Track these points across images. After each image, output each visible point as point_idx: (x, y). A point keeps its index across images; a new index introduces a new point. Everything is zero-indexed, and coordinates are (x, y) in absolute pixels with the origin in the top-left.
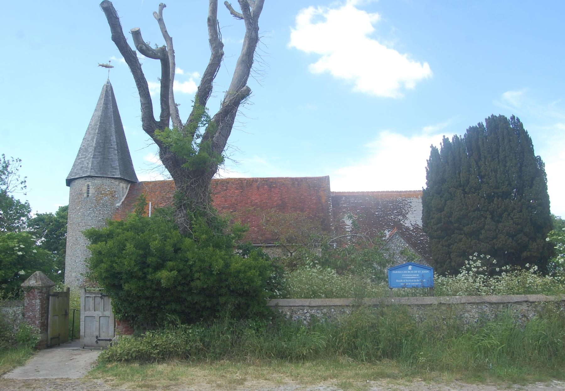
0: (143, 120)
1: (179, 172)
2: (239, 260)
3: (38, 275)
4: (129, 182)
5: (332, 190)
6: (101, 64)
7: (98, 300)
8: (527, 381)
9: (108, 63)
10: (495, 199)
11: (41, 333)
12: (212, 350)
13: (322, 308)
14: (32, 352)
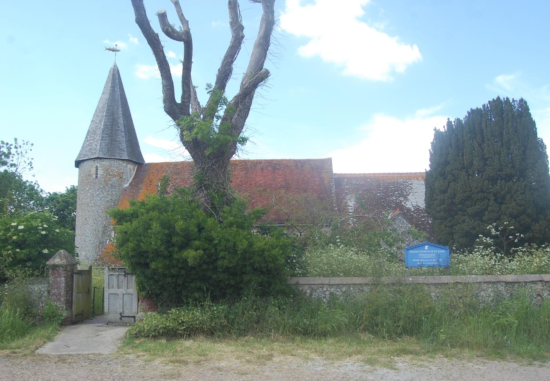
0: (165, 102)
1: (199, 153)
2: (262, 241)
3: (63, 253)
5: (334, 172)
6: (108, 48)
7: (122, 278)
8: (547, 358)
9: (115, 47)
10: (499, 181)
11: (66, 310)
12: (237, 327)
13: (341, 286)
14: (58, 327)
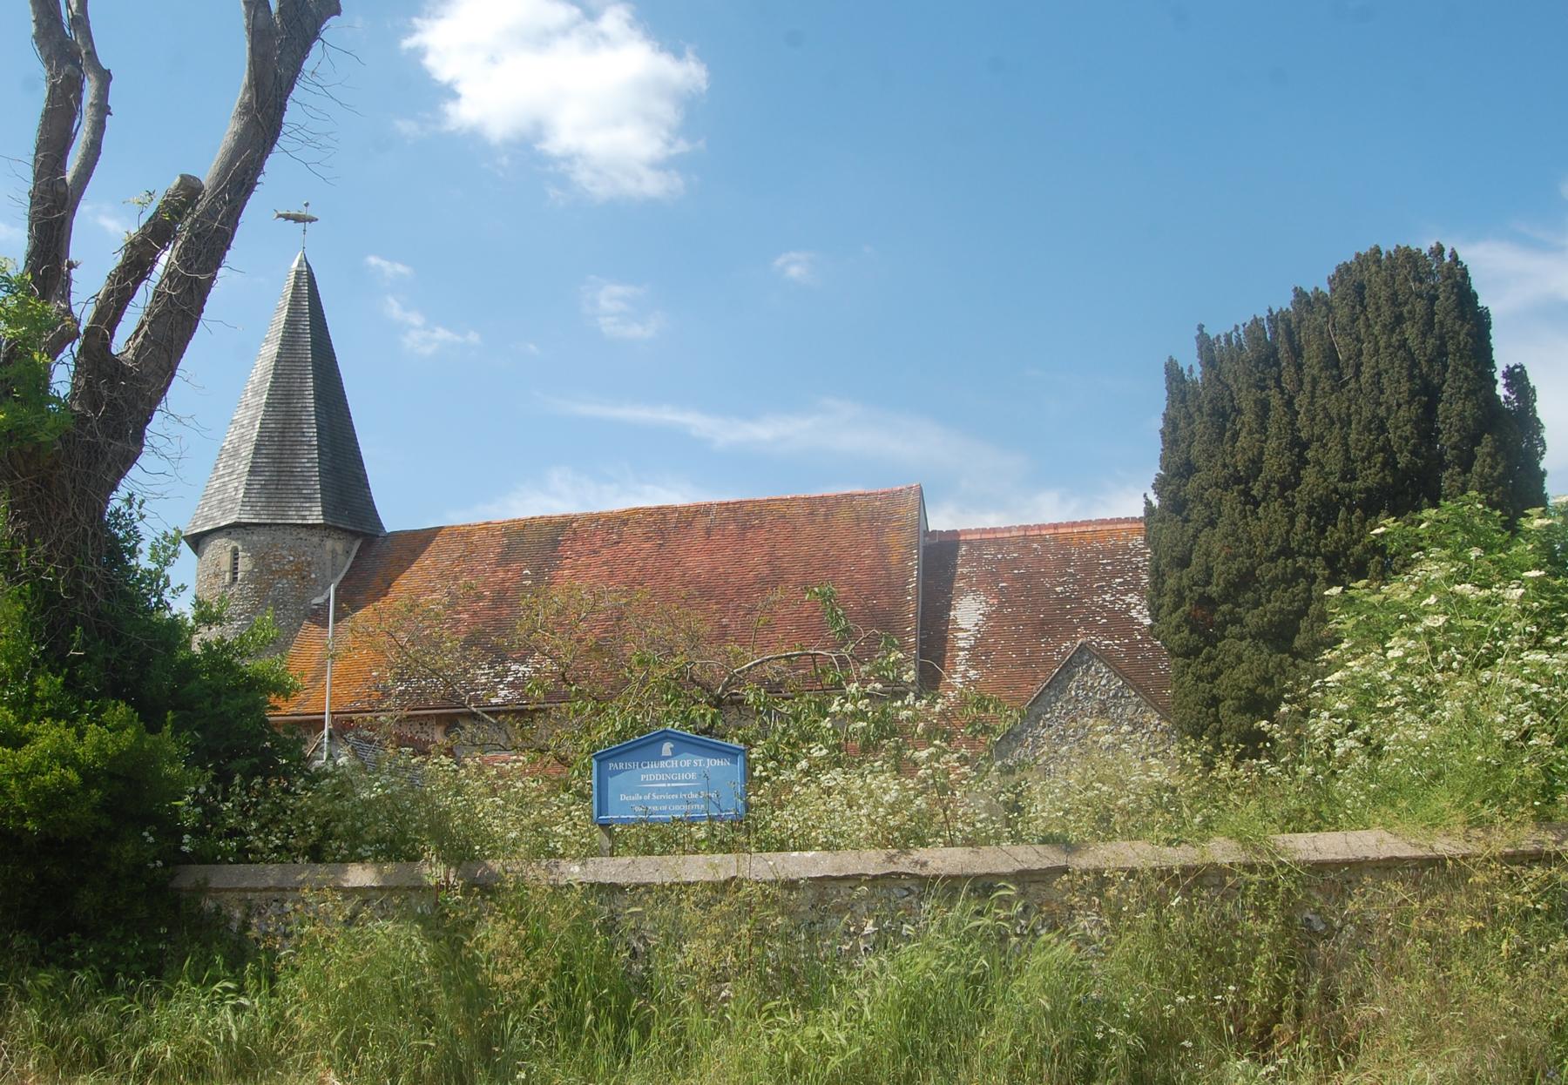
4: (355, 535)
